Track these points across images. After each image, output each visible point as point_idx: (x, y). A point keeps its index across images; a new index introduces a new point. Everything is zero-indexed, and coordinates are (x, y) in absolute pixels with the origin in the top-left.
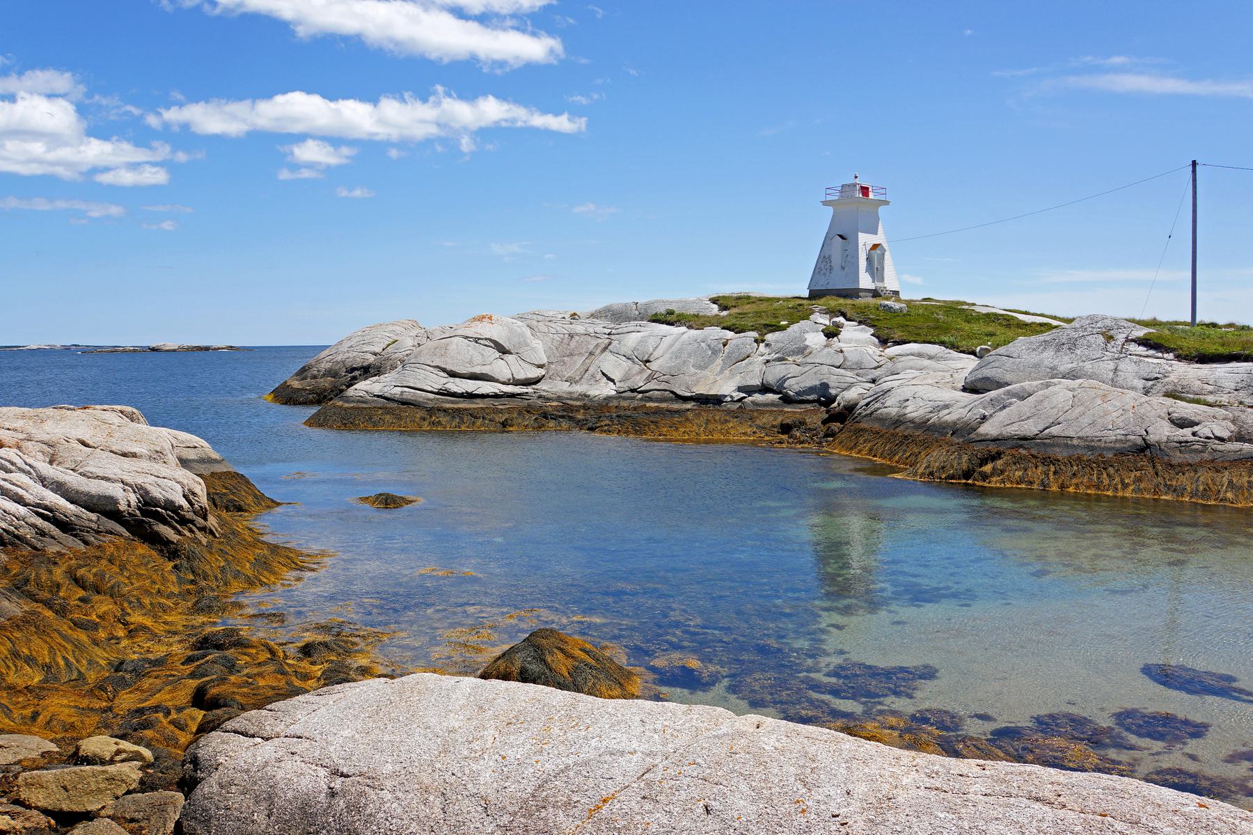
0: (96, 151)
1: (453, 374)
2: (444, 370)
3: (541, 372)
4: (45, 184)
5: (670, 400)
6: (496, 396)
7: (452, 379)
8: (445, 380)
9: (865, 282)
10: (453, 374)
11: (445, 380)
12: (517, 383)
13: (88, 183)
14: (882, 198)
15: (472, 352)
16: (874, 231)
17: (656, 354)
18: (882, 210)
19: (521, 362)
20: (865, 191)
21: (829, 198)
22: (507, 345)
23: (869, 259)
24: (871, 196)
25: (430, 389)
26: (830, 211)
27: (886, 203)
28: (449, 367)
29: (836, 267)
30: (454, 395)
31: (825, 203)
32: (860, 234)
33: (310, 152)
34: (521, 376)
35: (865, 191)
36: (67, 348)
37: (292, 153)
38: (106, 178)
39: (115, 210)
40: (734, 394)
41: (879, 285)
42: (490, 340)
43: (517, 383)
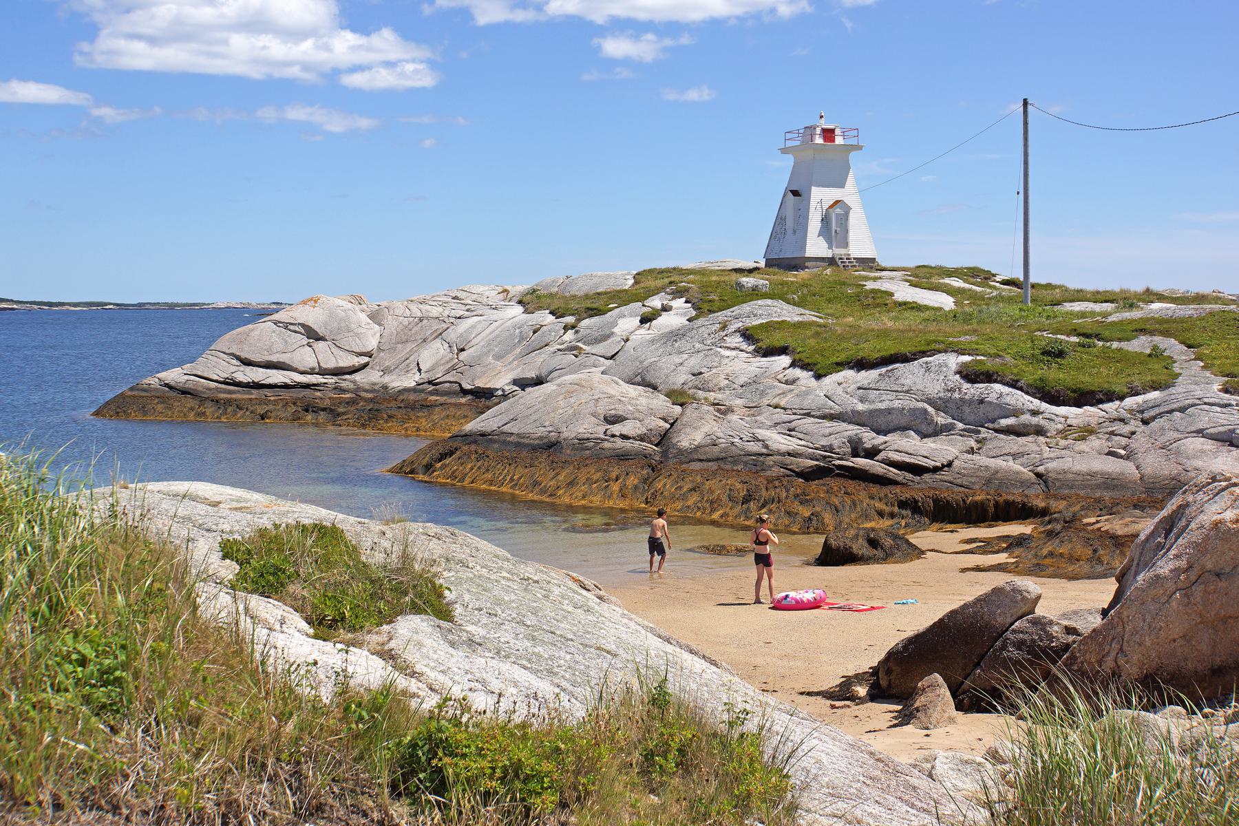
0: (345, 45)
1: (247, 363)
2: (238, 358)
3: (365, 360)
4: (277, 89)
5: (454, 393)
6: (286, 386)
7: (243, 368)
8: (233, 369)
9: (816, 247)
10: (247, 363)
11: (233, 369)
12: (323, 372)
13: (328, 87)
14: (853, 142)
15: (275, 338)
16: (841, 184)
17: (473, 343)
18: (853, 156)
19: (335, 350)
20: (828, 134)
21: (789, 144)
22: (321, 332)
23: (825, 220)
24: (839, 140)
25: (215, 377)
26: (789, 161)
27: (859, 148)
28: (243, 355)
29: (790, 231)
30: (239, 384)
31: (784, 151)
32: (814, 189)
33: (615, 47)
34: (331, 364)
35: (828, 134)
36: (140, 305)
37: (599, 47)
38: (357, 80)
39: (364, 123)
40: (506, 388)
41: (840, 251)
42: (303, 325)
43: (323, 372)
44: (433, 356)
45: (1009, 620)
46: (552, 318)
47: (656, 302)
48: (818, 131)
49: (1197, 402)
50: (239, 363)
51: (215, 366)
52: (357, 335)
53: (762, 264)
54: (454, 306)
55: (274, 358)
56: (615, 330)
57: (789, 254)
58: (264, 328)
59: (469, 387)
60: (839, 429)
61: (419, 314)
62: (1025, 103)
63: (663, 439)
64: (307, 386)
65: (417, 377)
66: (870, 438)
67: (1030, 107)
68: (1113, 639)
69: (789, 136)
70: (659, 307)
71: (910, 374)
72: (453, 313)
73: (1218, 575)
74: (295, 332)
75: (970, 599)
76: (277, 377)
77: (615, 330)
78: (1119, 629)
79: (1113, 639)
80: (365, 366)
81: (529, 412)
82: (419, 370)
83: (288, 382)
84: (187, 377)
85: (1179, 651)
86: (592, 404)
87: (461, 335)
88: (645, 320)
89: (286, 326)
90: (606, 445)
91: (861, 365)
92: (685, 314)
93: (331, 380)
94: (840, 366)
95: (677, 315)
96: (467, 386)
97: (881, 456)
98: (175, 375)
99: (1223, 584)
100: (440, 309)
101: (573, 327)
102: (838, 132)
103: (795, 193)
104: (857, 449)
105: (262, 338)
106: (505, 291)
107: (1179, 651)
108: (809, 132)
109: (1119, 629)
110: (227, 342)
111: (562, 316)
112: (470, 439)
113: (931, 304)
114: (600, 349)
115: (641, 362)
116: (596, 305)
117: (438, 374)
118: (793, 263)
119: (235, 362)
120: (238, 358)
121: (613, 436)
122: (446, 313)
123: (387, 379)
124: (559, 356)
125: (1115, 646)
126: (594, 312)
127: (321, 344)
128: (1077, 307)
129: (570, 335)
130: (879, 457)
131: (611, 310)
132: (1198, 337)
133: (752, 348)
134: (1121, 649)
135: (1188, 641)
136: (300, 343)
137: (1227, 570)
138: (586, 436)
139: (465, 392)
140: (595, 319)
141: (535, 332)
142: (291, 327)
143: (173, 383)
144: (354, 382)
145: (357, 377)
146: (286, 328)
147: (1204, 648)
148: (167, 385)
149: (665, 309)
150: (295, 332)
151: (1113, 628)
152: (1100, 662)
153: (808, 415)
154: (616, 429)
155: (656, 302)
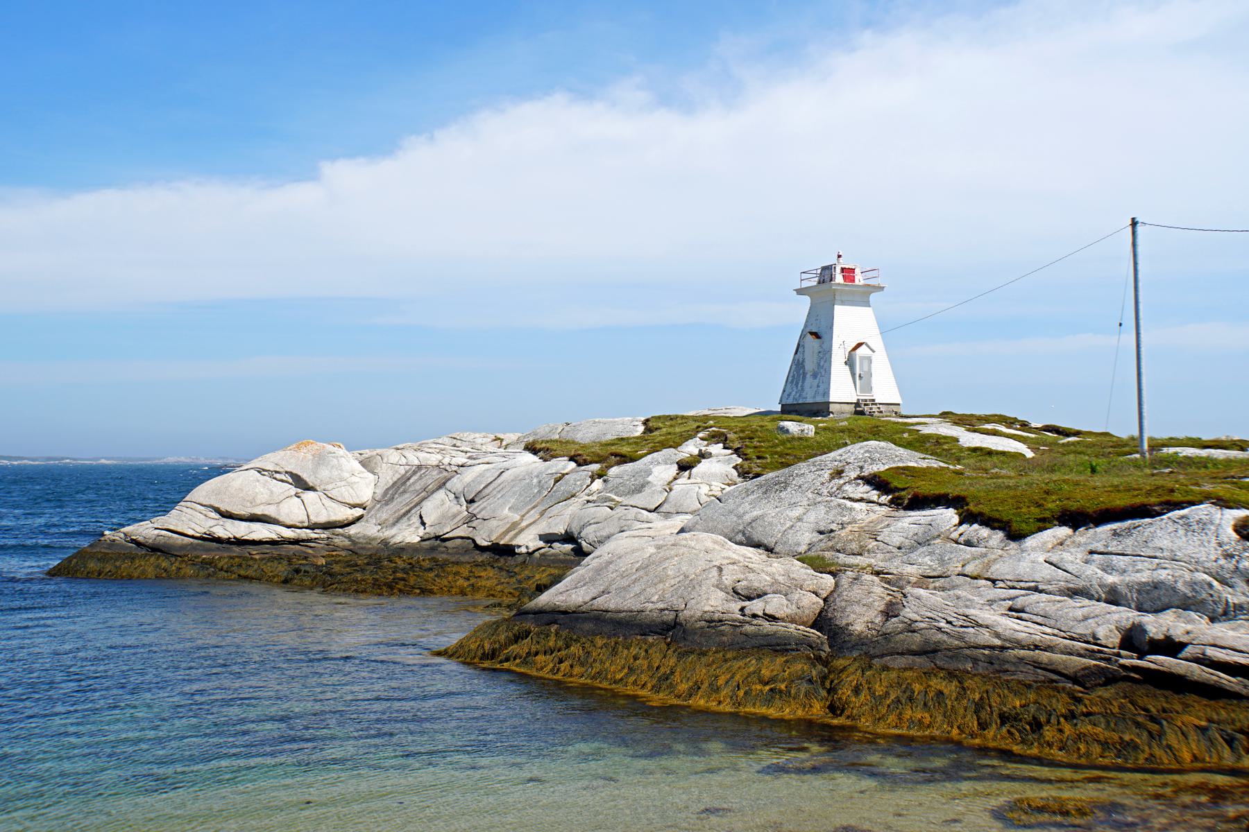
2: (217, 510)
3: (358, 512)
6: (273, 543)
8: (212, 523)
12: (313, 527)
21: (805, 284)
25: (190, 532)
26: (806, 301)
28: (223, 508)
30: (218, 540)
31: (800, 292)
42: (291, 474)
43: (313, 527)
44: (440, 513)
46: (573, 465)
47: (691, 448)
48: (838, 270)
50: (218, 516)
51: (190, 519)
52: (350, 485)
53: (779, 408)
54: (454, 453)
55: (258, 511)
56: (650, 479)
57: (809, 397)
58: (234, 480)
59: (485, 544)
61: (417, 462)
62: (1134, 223)
63: (821, 621)
64: (296, 542)
65: (421, 531)
66: (1157, 625)
67: (1139, 228)
69: (804, 276)
70: (696, 452)
71: (1162, 533)
72: (455, 461)
74: (282, 481)
76: (261, 532)
77: (650, 479)
80: (359, 518)
81: (625, 582)
82: (423, 524)
83: (275, 537)
84: (157, 532)
86: (715, 572)
87: (468, 485)
88: (684, 466)
89: (273, 474)
90: (748, 628)
91: (1076, 519)
92: (728, 462)
93: (324, 535)
94: (1043, 524)
95: (719, 465)
96: (483, 543)
97: (1188, 652)
98: (146, 530)
100: (439, 457)
101: (600, 476)
102: (857, 271)
103: (816, 335)
104: (1133, 639)
105: (246, 488)
106: (497, 439)
108: (827, 272)
110: (203, 492)
111: (586, 463)
112: (546, 618)
113: (1000, 449)
114: (637, 499)
115: (740, 517)
116: (618, 454)
117: (444, 530)
118: (815, 408)
119: (214, 515)
120: (217, 510)
121: (755, 616)
122: (446, 461)
123: (387, 533)
124: (591, 509)
126: (624, 459)
127: (310, 494)
128: (1172, 450)
129: (598, 484)
130: (1183, 654)
131: (642, 457)
133: (885, 499)
136: (287, 494)
138: (716, 616)
139: (483, 549)
140: (629, 467)
141: (557, 481)
142: (278, 476)
143: (140, 539)
144: (349, 537)
145: (352, 530)
148: (133, 541)
149: (702, 456)
150: (282, 481)
153: (1036, 589)
154: (756, 606)
155: (691, 448)
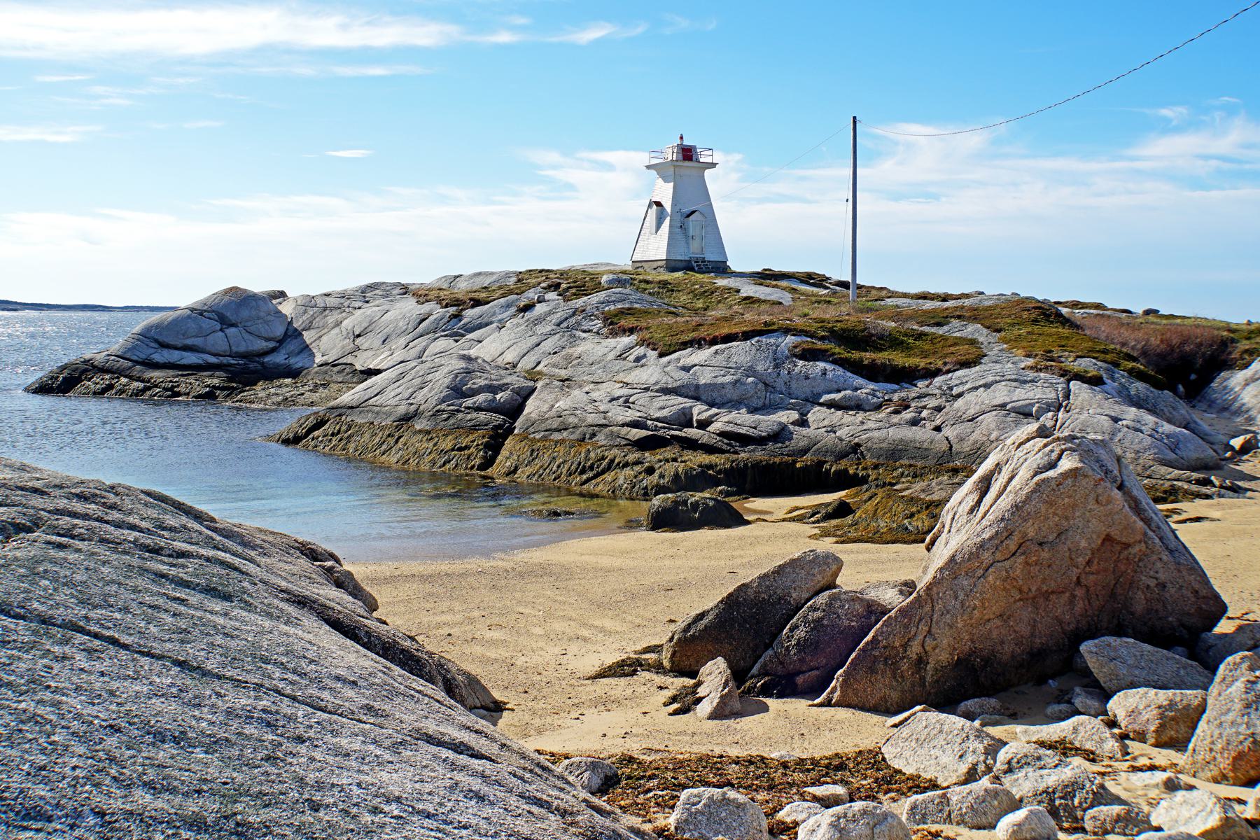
2: (156, 341)
19: (246, 336)
45: (806, 595)
49: (998, 378)
55: (189, 342)
60: (671, 402)
66: (699, 411)
68: (920, 620)
73: (1041, 544)
75: (731, 590)
78: (927, 608)
79: (920, 620)
85: (995, 634)
99: (1045, 555)
107: (995, 634)
109: (927, 608)
119: (153, 345)
120: (156, 341)
125: (923, 628)
132: (1002, 323)
134: (929, 632)
135: (1005, 621)
137: (1051, 538)
146: (201, 314)
147: (1025, 630)
149: (541, 300)
151: (921, 607)
152: (905, 646)
